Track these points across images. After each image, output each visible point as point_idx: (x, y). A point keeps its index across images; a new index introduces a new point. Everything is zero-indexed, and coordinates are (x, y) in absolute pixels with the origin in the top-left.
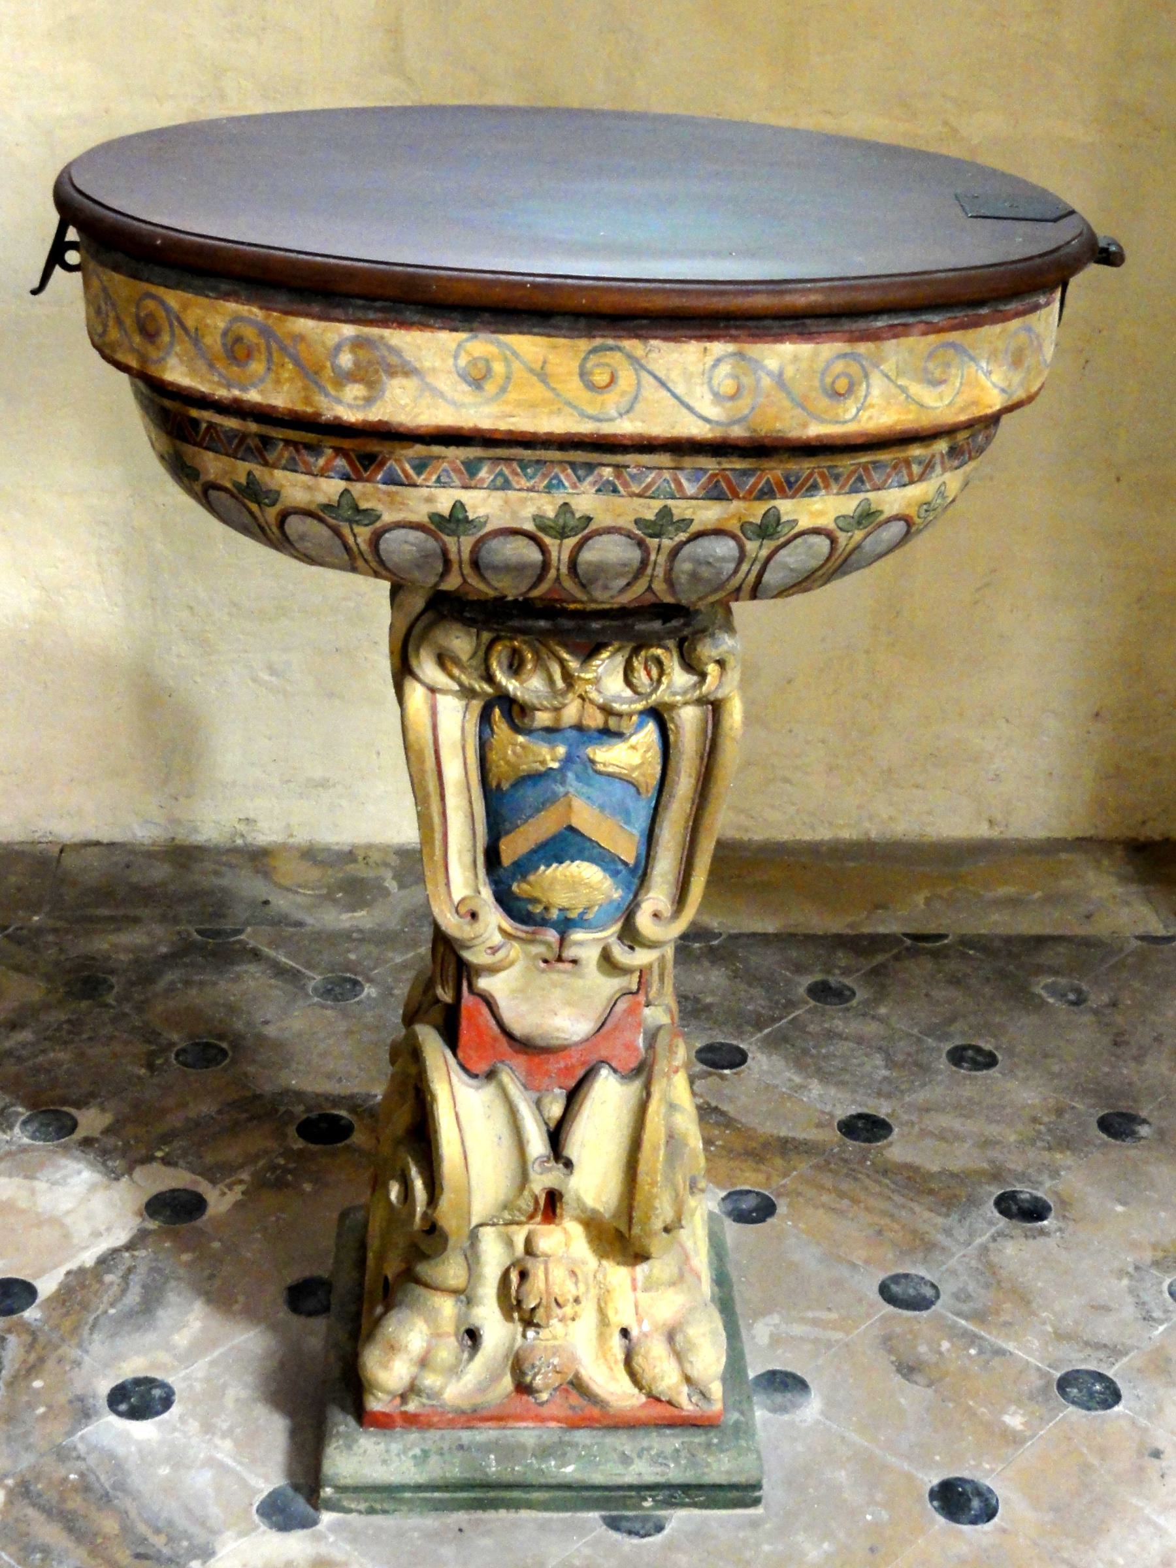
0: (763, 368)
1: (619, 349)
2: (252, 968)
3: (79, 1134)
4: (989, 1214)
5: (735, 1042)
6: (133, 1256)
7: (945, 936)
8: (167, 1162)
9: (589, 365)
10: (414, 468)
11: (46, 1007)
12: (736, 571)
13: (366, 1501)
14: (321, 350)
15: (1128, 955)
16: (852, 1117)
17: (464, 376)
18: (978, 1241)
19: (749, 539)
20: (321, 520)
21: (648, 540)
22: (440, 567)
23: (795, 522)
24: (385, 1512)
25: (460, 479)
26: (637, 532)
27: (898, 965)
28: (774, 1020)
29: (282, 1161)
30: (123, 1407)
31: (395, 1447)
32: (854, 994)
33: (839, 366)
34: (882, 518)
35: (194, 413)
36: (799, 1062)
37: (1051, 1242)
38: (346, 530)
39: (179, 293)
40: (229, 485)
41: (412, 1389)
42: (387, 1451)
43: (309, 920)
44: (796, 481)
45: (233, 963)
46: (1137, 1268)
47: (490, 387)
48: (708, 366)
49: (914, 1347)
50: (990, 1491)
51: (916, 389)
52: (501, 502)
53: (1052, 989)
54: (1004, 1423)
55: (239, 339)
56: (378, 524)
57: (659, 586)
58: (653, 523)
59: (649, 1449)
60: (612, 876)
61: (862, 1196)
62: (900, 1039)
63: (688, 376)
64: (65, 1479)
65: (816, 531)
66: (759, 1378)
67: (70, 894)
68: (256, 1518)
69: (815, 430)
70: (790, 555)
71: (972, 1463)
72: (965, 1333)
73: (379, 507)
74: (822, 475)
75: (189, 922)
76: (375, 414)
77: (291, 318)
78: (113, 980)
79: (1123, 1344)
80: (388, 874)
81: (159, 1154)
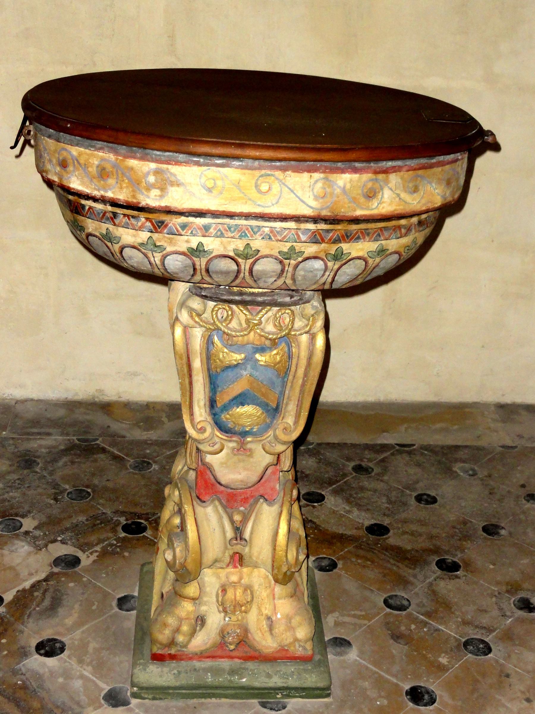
0: (336, 184)
1: (272, 175)
2: (102, 456)
3: (23, 530)
4: (433, 569)
5: (319, 491)
6: (47, 584)
7: (414, 445)
8: (63, 542)
9: (259, 182)
10: (181, 227)
11: (9, 473)
12: (323, 275)
13: (152, 694)
14: (140, 174)
15: (496, 454)
16: (372, 525)
17: (204, 187)
18: (428, 581)
19: (329, 261)
20: (139, 250)
21: (285, 261)
22: (192, 272)
23: (350, 253)
24: (161, 699)
25: (201, 232)
26: (280, 257)
27: (393, 457)
28: (338, 482)
29: (115, 542)
30: (42, 652)
31: (166, 670)
32: (373, 470)
33: (370, 185)
34: (388, 252)
35: (83, 202)
36: (348, 501)
37: (460, 581)
38: (150, 255)
39: (77, 148)
40: (98, 234)
41: (172, 643)
42: (162, 671)
43: (128, 435)
44: (351, 235)
45: (93, 454)
46: (499, 593)
47: (215, 192)
48: (312, 184)
49: (399, 627)
50: (433, 692)
51: (403, 195)
52: (219, 243)
53: (462, 469)
54: (439, 661)
55: (104, 169)
56: (164, 252)
57: (289, 282)
58: (287, 253)
59: (280, 671)
60: (266, 412)
61: (376, 560)
62: (394, 491)
63: (303, 188)
64: (16, 684)
65: (359, 258)
66: (330, 640)
67: (20, 423)
68: (103, 702)
69: (359, 213)
70: (347, 269)
71: (425, 679)
72: (422, 621)
73: (165, 245)
74: (362, 233)
75: (74, 435)
76: (163, 203)
77: (128, 160)
78: (39, 460)
79: (493, 627)
80: (164, 415)
81: (59, 539)
